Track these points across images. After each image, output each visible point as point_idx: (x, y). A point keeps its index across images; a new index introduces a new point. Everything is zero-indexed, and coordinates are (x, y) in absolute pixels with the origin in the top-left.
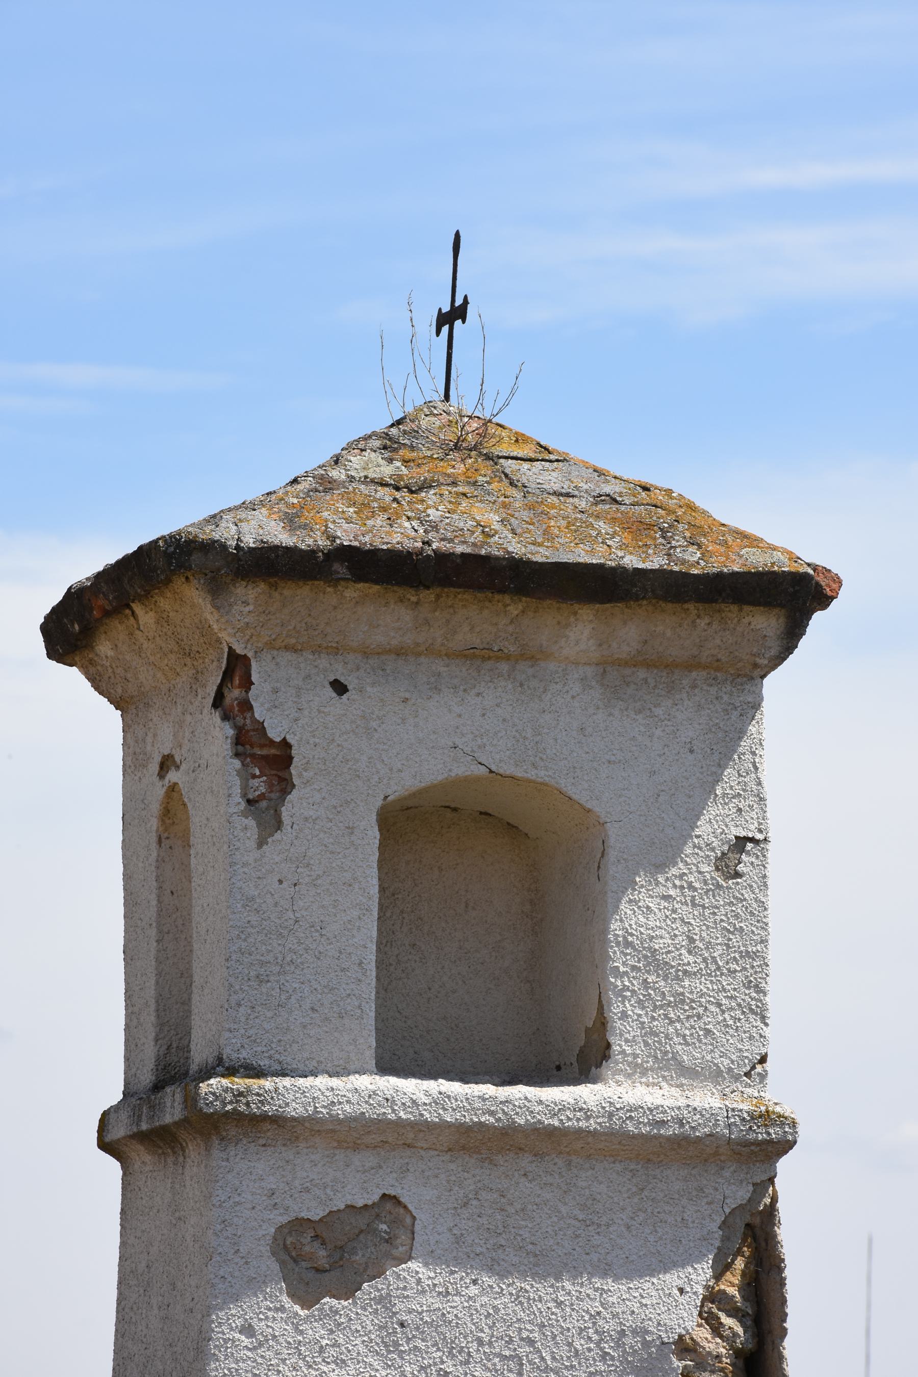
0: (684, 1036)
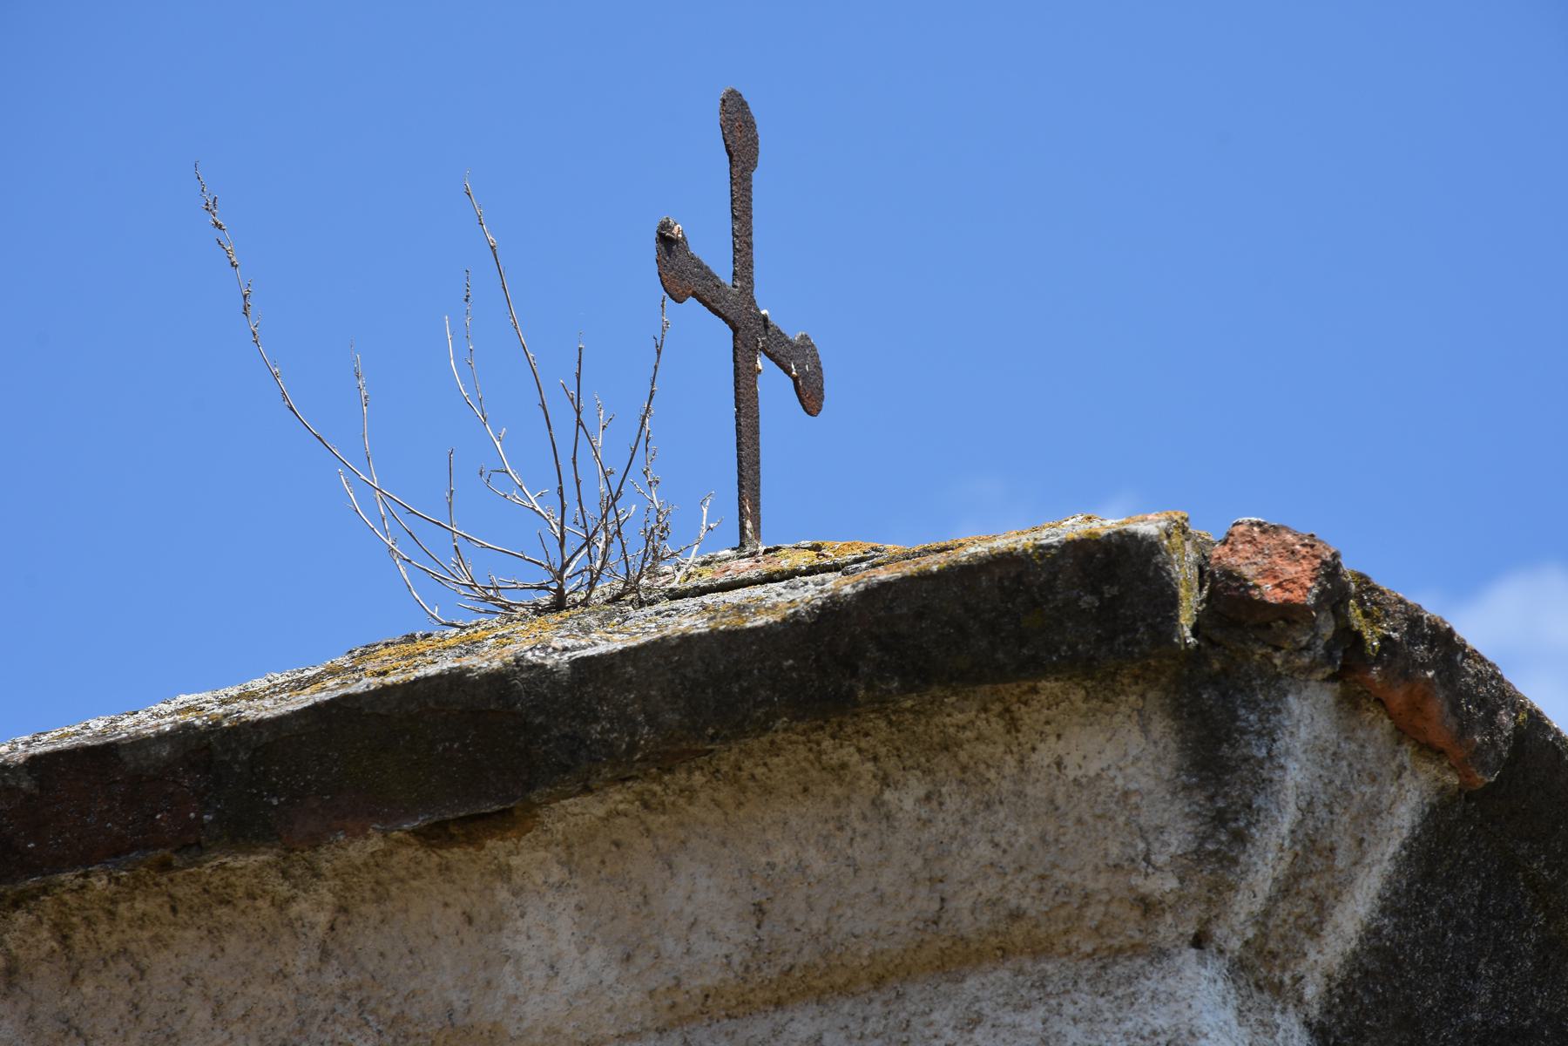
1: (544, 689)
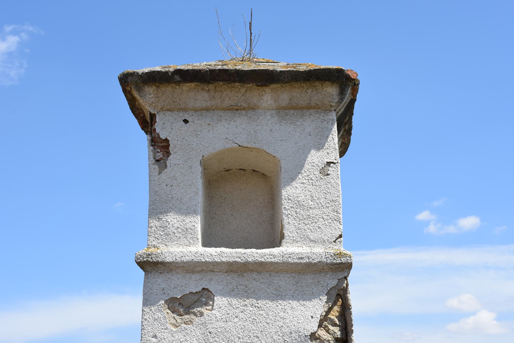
0: (311, 230)
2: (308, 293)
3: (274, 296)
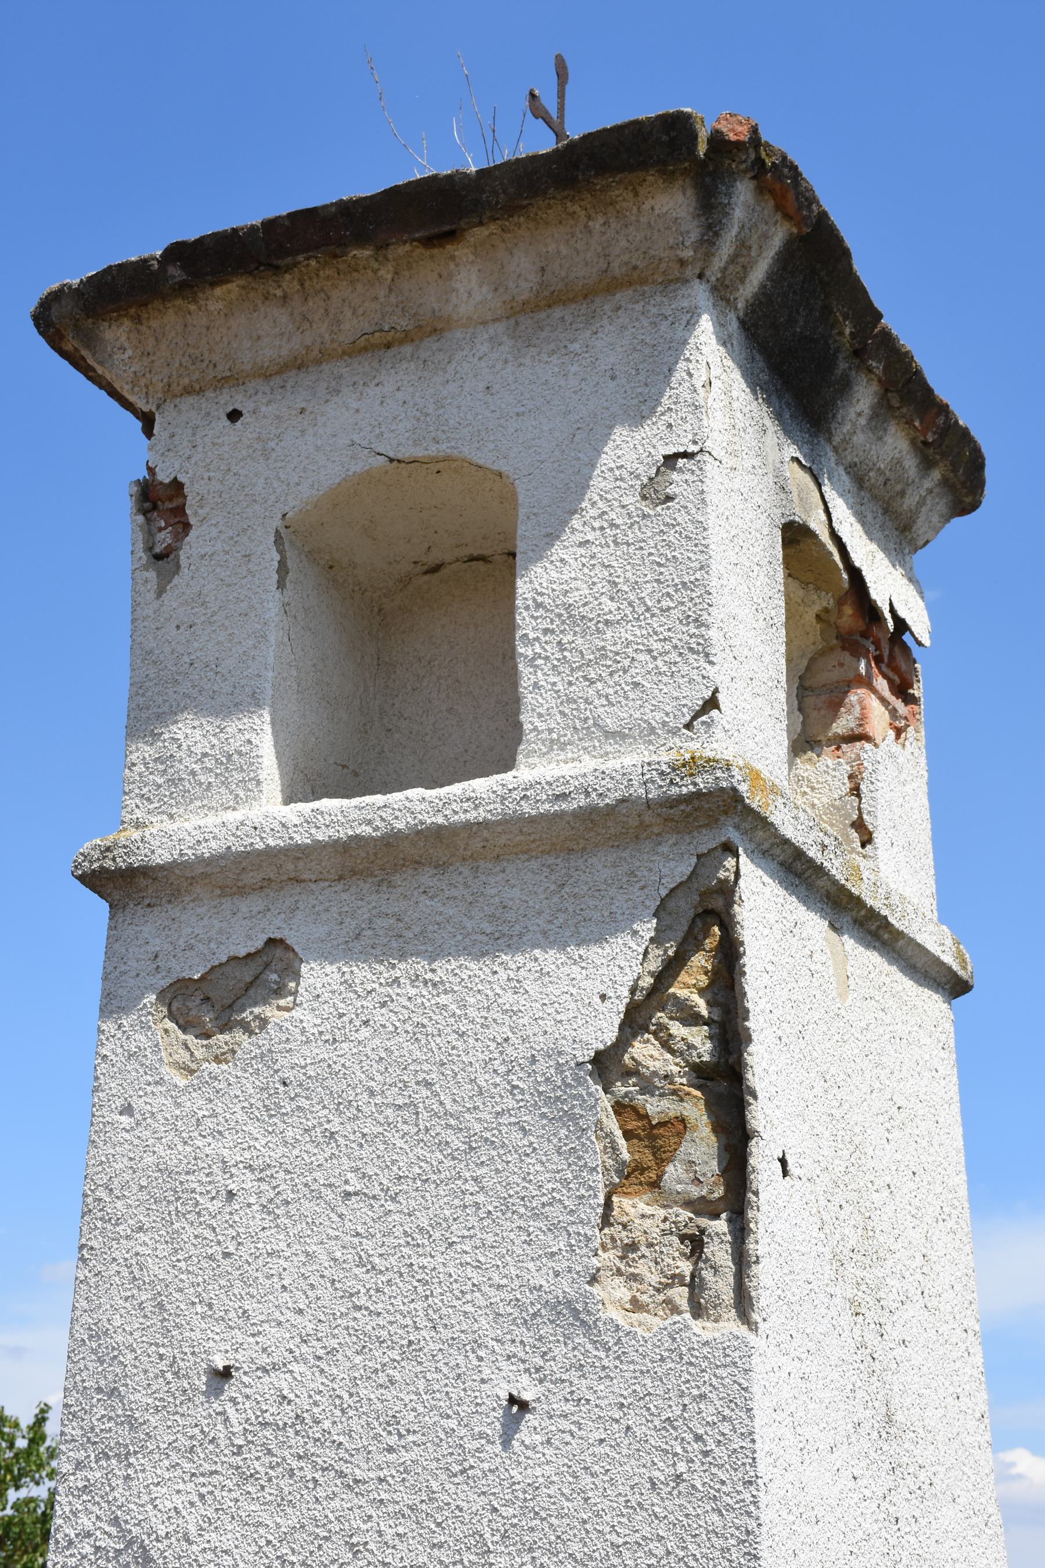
1: (466, 181)
2: (596, 916)
3: (485, 939)
